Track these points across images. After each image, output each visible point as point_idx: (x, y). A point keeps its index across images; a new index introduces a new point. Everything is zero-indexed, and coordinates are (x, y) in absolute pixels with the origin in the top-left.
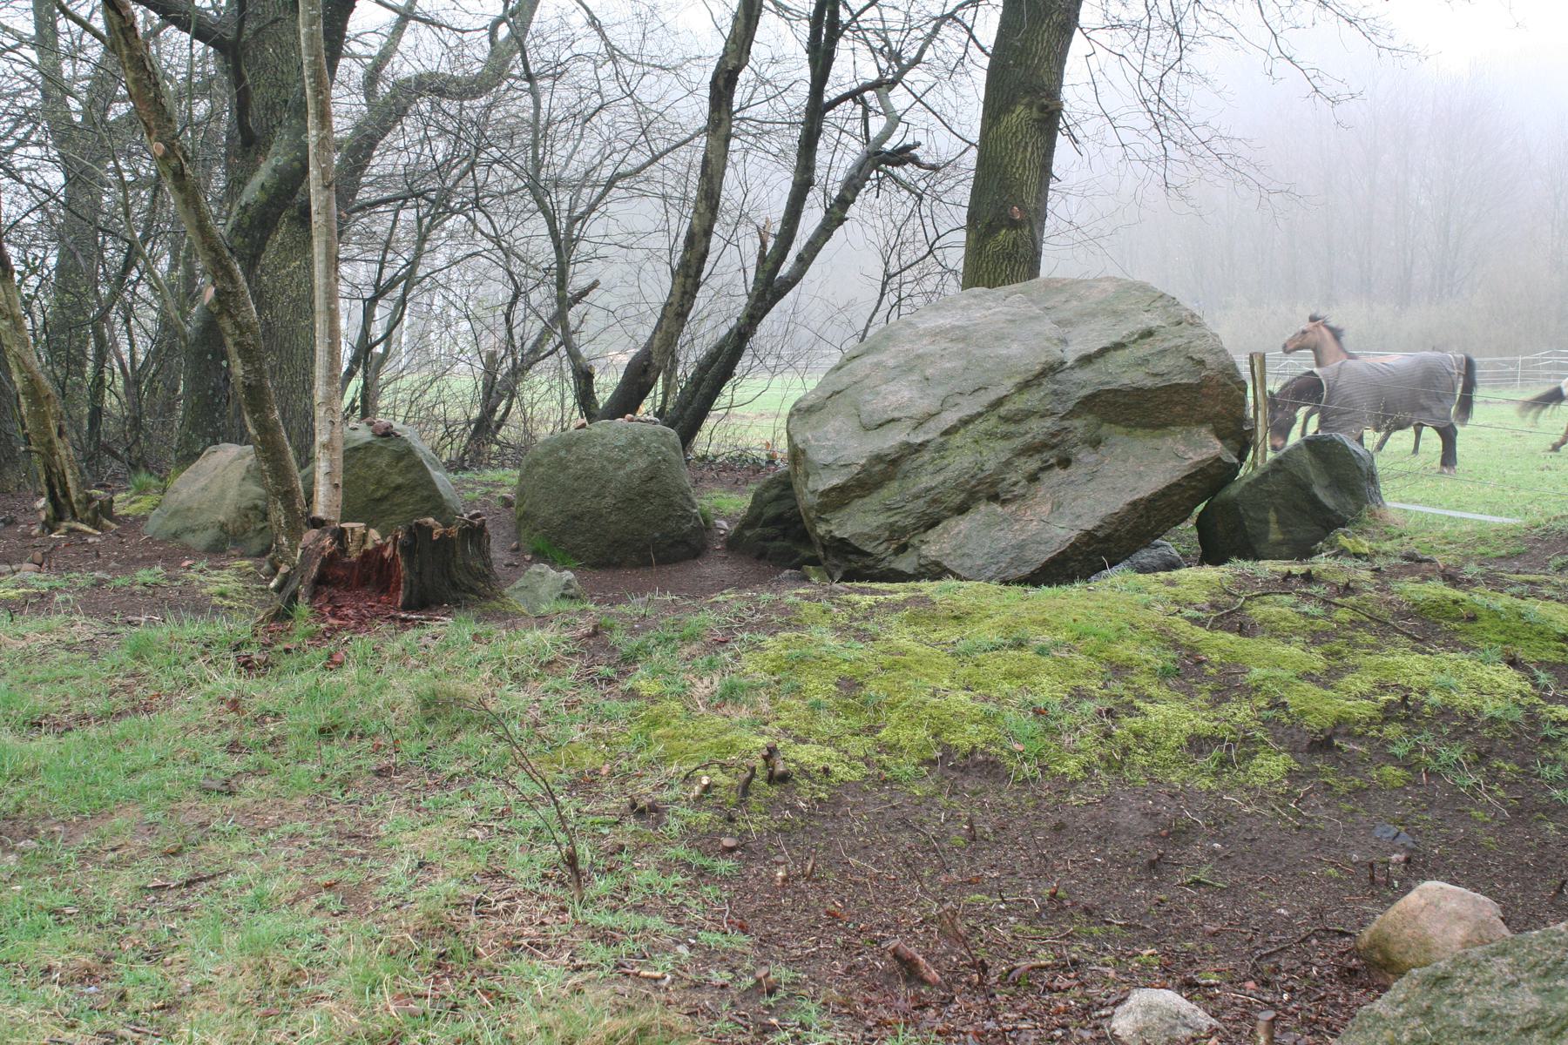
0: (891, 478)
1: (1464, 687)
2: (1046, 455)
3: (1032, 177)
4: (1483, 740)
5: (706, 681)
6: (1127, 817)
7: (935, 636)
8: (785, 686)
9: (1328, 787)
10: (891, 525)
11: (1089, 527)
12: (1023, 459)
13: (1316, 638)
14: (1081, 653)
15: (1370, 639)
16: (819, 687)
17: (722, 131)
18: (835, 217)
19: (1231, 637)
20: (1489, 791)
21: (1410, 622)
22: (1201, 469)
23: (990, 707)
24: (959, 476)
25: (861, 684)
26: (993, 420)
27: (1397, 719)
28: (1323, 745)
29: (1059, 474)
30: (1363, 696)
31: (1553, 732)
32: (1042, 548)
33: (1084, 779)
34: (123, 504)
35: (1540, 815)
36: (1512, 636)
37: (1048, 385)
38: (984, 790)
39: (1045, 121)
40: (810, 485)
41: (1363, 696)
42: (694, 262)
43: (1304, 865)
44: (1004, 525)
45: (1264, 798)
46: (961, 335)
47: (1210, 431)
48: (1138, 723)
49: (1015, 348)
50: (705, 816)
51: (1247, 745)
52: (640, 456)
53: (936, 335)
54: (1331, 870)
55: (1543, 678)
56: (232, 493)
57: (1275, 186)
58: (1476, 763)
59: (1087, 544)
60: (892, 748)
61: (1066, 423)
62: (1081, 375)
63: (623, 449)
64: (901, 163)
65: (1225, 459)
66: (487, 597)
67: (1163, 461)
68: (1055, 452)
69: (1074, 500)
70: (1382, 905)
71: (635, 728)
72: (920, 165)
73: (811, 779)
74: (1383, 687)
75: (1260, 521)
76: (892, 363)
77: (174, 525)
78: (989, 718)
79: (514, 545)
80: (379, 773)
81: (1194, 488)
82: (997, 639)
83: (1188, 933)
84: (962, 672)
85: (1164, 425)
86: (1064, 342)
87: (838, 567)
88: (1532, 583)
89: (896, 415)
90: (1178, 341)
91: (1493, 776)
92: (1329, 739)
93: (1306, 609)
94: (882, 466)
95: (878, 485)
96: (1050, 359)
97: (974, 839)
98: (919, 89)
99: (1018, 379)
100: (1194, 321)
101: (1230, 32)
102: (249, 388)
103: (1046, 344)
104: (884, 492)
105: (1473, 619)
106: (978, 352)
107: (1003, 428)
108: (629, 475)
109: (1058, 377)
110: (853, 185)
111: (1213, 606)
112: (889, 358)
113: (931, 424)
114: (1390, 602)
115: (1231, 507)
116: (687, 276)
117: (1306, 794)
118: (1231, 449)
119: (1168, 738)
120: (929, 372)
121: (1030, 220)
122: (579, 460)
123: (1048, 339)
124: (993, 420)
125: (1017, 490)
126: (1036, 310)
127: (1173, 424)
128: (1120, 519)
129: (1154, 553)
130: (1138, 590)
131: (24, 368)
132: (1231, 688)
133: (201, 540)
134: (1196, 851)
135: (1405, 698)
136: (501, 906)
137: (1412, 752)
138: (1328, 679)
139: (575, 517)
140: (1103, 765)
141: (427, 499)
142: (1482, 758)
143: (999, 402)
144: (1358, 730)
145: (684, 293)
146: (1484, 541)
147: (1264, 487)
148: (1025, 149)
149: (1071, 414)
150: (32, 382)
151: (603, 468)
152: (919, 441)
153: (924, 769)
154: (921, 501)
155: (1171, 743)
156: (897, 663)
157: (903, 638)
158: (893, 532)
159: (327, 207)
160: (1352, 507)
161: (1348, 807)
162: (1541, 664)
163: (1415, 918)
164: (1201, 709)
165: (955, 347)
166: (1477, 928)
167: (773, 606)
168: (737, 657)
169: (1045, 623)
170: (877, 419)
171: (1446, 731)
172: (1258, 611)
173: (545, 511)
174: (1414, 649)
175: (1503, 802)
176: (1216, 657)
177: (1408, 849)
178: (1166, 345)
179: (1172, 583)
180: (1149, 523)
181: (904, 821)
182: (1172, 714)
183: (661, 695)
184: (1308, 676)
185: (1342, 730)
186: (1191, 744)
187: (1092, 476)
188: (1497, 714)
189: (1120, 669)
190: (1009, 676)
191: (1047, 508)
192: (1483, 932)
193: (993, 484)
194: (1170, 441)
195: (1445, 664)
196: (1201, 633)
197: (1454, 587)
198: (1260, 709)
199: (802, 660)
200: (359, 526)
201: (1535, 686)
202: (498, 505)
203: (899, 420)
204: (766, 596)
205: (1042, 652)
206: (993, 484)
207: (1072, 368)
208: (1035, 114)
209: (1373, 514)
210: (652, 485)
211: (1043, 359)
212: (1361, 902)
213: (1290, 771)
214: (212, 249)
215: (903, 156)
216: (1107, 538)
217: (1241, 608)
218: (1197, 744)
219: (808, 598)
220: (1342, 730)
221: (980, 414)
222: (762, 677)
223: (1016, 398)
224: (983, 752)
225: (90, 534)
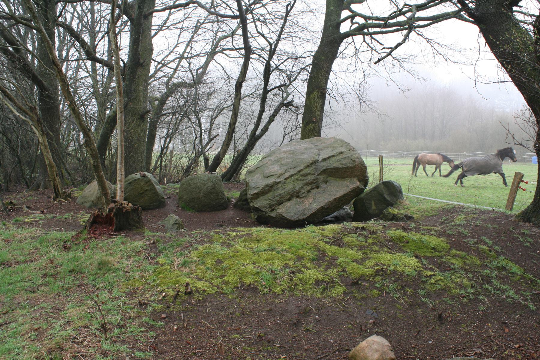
0: (270, 191)
1: (401, 264)
2: (312, 185)
3: (319, 110)
4: (404, 281)
5: (179, 260)
6: (291, 307)
7: (250, 246)
8: (201, 262)
9: (355, 297)
11: (322, 205)
13: (361, 248)
14: (290, 253)
15: (377, 248)
16: (210, 262)
17: (238, 97)
18: (272, 119)
19: (336, 247)
20: (403, 299)
21: (389, 243)
23: (258, 270)
25: (223, 262)
26: (299, 176)
27: (379, 275)
28: (355, 283)
30: (371, 267)
31: (424, 279)
33: (282, 294)
34: (76, 193)
35: (417, 306)
36: (418, 248)
37: (314, 167)
38: (252, 297)
40: (249, 192)
41: (371, 267)
42: (231, 131)
43: (342, 324)
45: (335, 301)
46: (292, 153)
48: (301, 276)
49: (306, 156)
50: (160, 306)
51: (332, 283)
54: (350, 326)
55: (424, 261)
56: (96, 193)
57: (382, 113)
58: (400, 289)
60: (227, 283)
61: (318, 177)
63: (206, 181)
66: (138, 228)
70: (362, 338)
71: (154, 274)
72: (293, 106)
73: (199, 293)
74: (377, 264)
76: (273, 160)
77: (82, 200)
78: (257, 274)
80: (79, 286)
82: (267, 248)
83: (299, 349)
84: (253, 258)
85: (344, 178)
86: (319, 155)
88: (429, 229)
90: (349, 155)
91: (405, 294)
92: (357, 282)
93: (360, 239)
94: (268, 188)
95: (267, 193)
97: (243, 314)
98: (295, 86)
99: (306, 165)
100: (354, 150)
101: (378, 74)
102: (94, 166)
104: (269, 195)
105: (407, 242)
106: (296, 157)
107: (301, 178)
110: (276, 112)
111: (333, 237)
112: (273, 158)
113: (282, 177)
114: (385, 237)
117: (348, 299)
119: (309, 281)
120: (283, 162)
122: (194, 184)
123: (315, 154)
125: (304, 195)
126: (313, 146)
127: (347, 177)
128: (331, 203)
129: (344, 211)
130: (313, 232)
131: (48, 159)
132: (332, 264)
133: (87, 205)
134: (310, 319)
135: (382, 268)
136: (81, 340)
137: (382, 286)
138: (360, 262)
140: (289, 289)
141: (154, 193)
142: (403, 287)
143: (300, 171)
144: (367, 278)
146: (427, 211)
149: (320, 174)
150: (50, 162)
153: (235, 290)
155: (310, 282)
156: (236, 255)
157: (240, 247)
158: (270, 206)
159: (121, 117)
160: (395, 200)
161: (360, 304)
162: (426, 257)
163: (364, 350)
164: (321, 271)
165: (290, 156)
166: (382, 355)
167: (206, 236)
168: (190, 252)
169: (282, 243)
170: (268, 175)
171: (393, 279)
172: (346, 239)
174: (388, 252)
175: (406, 302)
176: (330, 254)
177: (376, 319)
179: (323, 230)
181: (224, 307)
182: (312, 273)
183: (165, 264)
184: (355, 261)
185: (362, 278)
186: (316, 283)
187: (324, 191)
188: (409, 273)
189: (300, 258)
190: (267, 260)
191: (311, 200)
192: (384, 356)
193: (298, 193)
195: (397, 257)
196: (327, 246)
197: (405, 232)
198: (339, 272)
199: (207, 254)
200: (126, 202)
201: (422, 264)
202: (175, 194)
204: (205, 232)
205: (278, 252)
206: (298, 193)
208: (319, 94)
209: (400, 202)
212: (356, 337)
213: (344, 292)
214: (83, 129)
215: (290, 104)
216: (328, 208)
217: (341, 238)
218: (318, 283)
219: (217, 233)
220: (362, 278)
221: (295, 174)
222: (195, 259)
223: (305, 170)
224: (253, 285)
225: (63, 202)
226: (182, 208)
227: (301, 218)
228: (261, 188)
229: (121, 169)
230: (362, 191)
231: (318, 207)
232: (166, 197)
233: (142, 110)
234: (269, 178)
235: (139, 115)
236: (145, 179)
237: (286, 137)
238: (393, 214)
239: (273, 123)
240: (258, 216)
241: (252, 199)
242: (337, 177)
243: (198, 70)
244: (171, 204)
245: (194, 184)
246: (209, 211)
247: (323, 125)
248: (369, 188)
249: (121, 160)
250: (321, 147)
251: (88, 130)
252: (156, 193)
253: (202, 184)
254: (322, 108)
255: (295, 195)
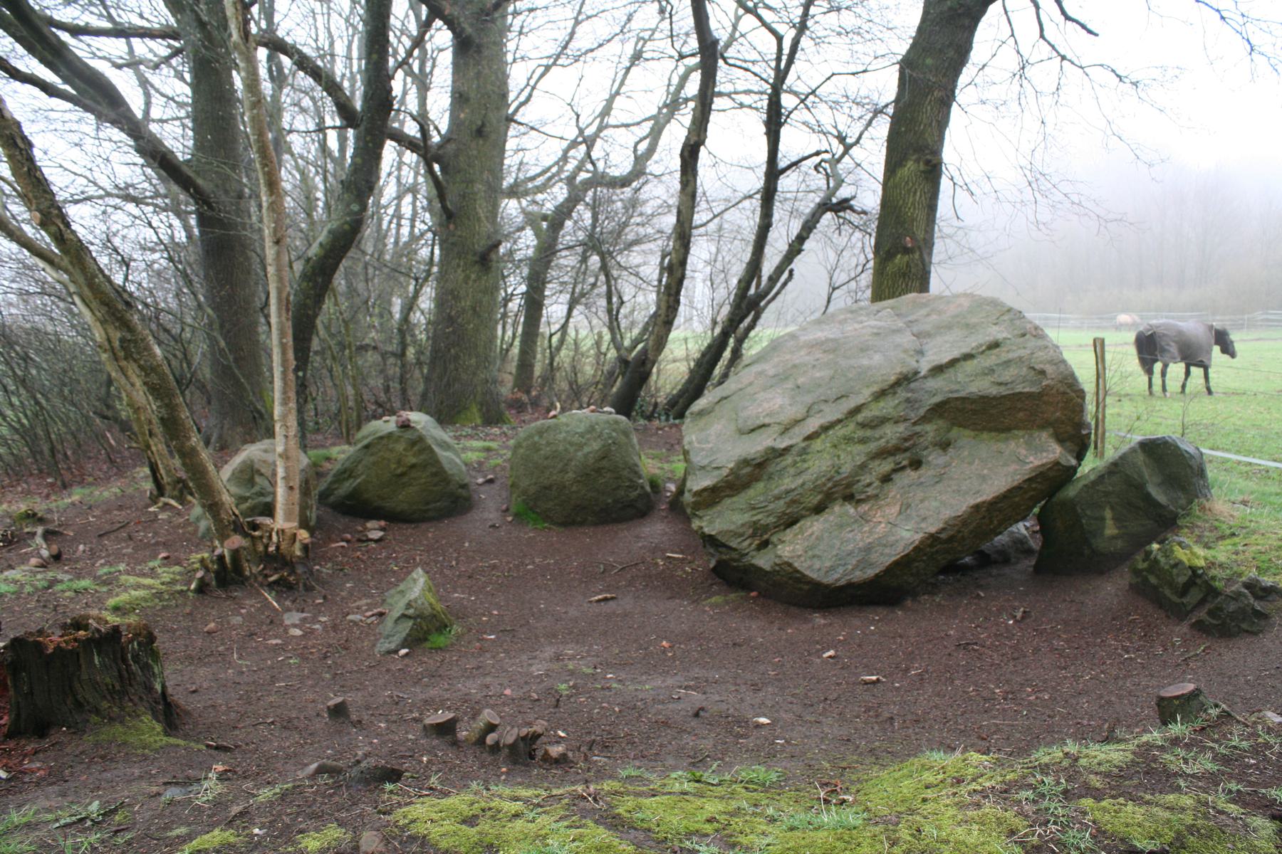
0: (757, 480)
2: (898, 458)
3: (921, 215)
10: (755, 523)
11: (933, 530)
12: (877, 462)
17: (689, 189)
18: (795, 248)
22: (1041, 473)
24: (817, 479)
26: (852, 426)
29: (911, 475)
32: (887, 551)
37: (902, 394)
39: (930, 172)
44: (855, 526)
47: (1051, 436)
49: (877, 358)
52: (595, 440)
53: (812, 346)
59: (931, 546)
61: (918, 428)
62: (932, 384)
63: (582, 435)
64: (844, 209)
65: (1063, 462)
67: (1005, 465)
68: (908, 454)
69: (922, 501)
72: (854, 211)
75: (1096, 519)
76: (772, 372)
79: (504, 507)
81: (1034, 489)
85: (1008, 430)
86: (920, 353)
87: (713, 556)
89: (767, 421)
90: (1022, 353)
95: (746, 485)
96: (905, 370)
99: (876, 388)
103: (902, 355)
104: (751, 492)
107: (860, 433)
108: (586, 456)
109: (913, 385)
110: (809, 227)
113: (796, 430)
115: (1069, 506)
116: (669, 295)
118: (1070, 451)
120: (801, 381)
121: (919, 248)
122: (548, 444)
123: (905, 351)
124: (852, 426)
125: (870, 491)
139: (546, 488)
141: (435, 474)
145: (669, 307)
147: (1100, 488)
148: (915, 193)
149: (924, 419)
151: (566, 450)
152: (783, 446)
154: (782, 502)
158: (756, 530)
160: (1183, 502)
173: (524, 483)
178: (1011, 356)
180: (991, 522)
187: (940, 478)
193: (849, 485)
194: (1012, 445)
203: (769, 425)
206: (849, 485)
207: (925, 377)
208: (922, 167)
209: (1203, 508)
210: (605, 463)
211: (898, 370)
215: (844, 205)
216: (951, 539)
221: (840, 421)
223: (873, 406)
226: (516, 515)
227: (858, 576)
228: (725, 472)
229: (284, 417)
230: (1067, 474)
231: (918, 537)
232: (480, 480)
233: (483, 242)
234: (753, 435)
235: (475, 254)
236: (408, 435)
237: (836, 293)
238: (1194, 569)
239: (799, 257)
240: (719, 563)
241: (697, 506)
242: (983, 429)
243: (637, 144)
244: (490, 508)
245: (548, 444)
246: (595, 524)
247: (935, 259)
248: (1090, 465)
249: (285, 392)
250: (927, 326)
251: (121, 306)
252: (440, 474)
253: (571, 444)
254: (932, 207)
255: (841, 491)
